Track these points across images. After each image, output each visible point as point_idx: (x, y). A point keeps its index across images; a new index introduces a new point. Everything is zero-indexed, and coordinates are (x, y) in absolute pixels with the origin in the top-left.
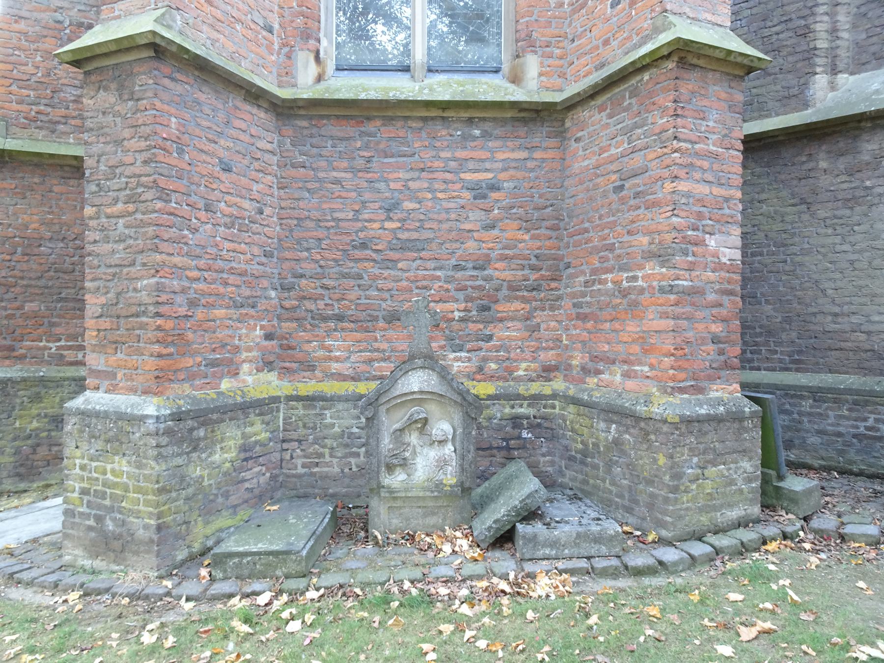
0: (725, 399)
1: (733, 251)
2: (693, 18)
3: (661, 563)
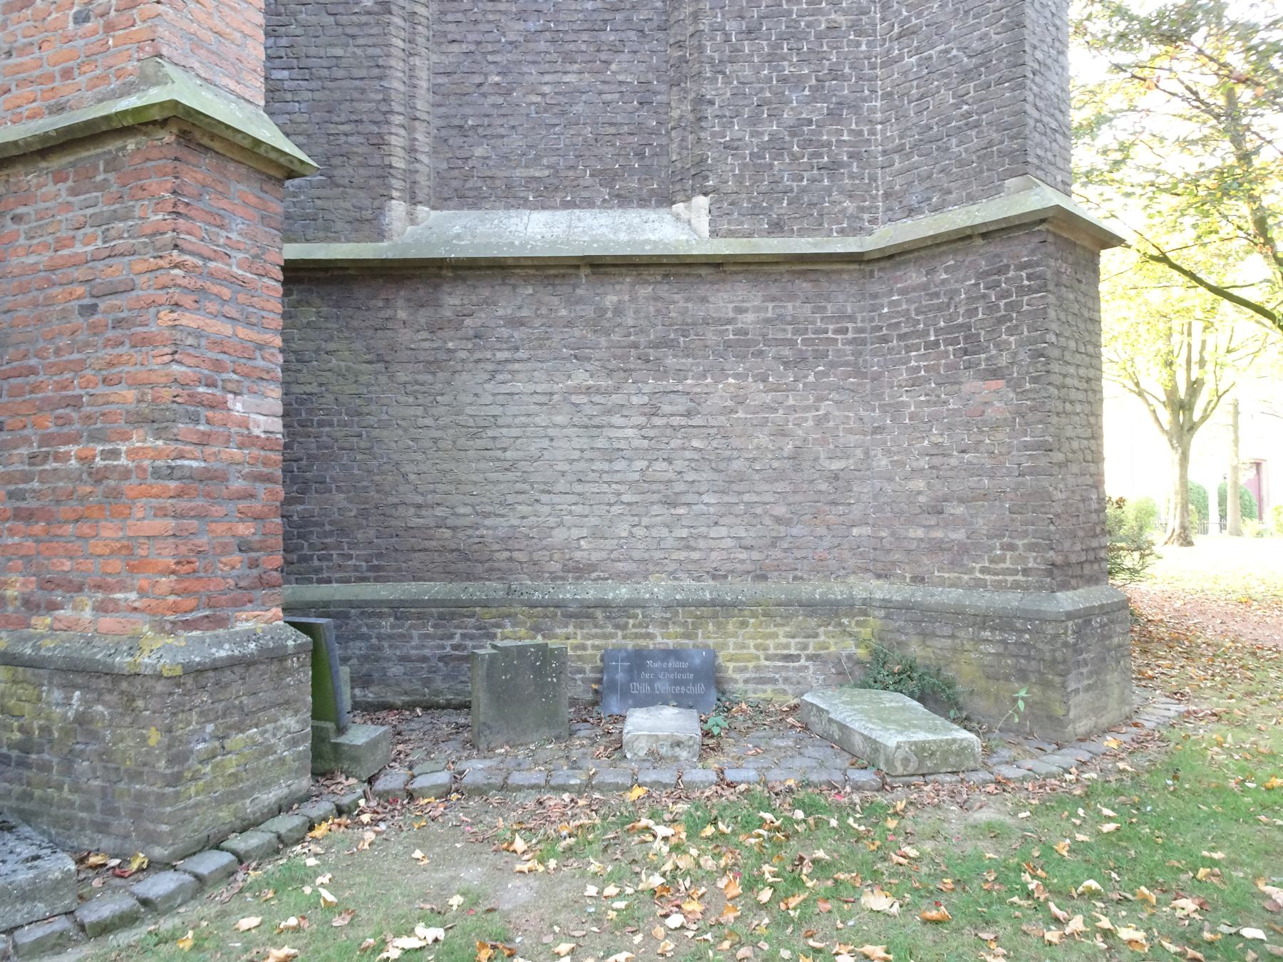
0: (259, 631)
1: (270, 419)
2: (206, 79)
3: (145, 902)
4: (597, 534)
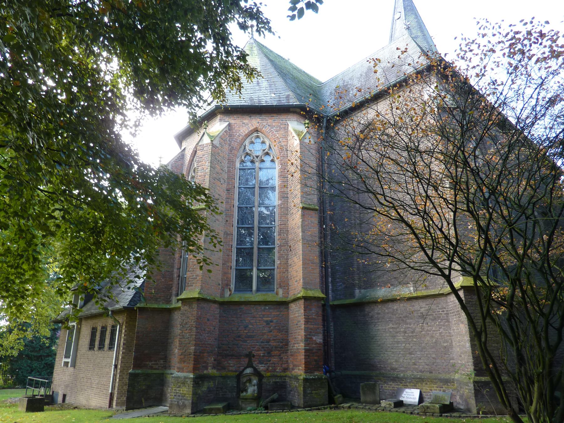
4: (396, 361)
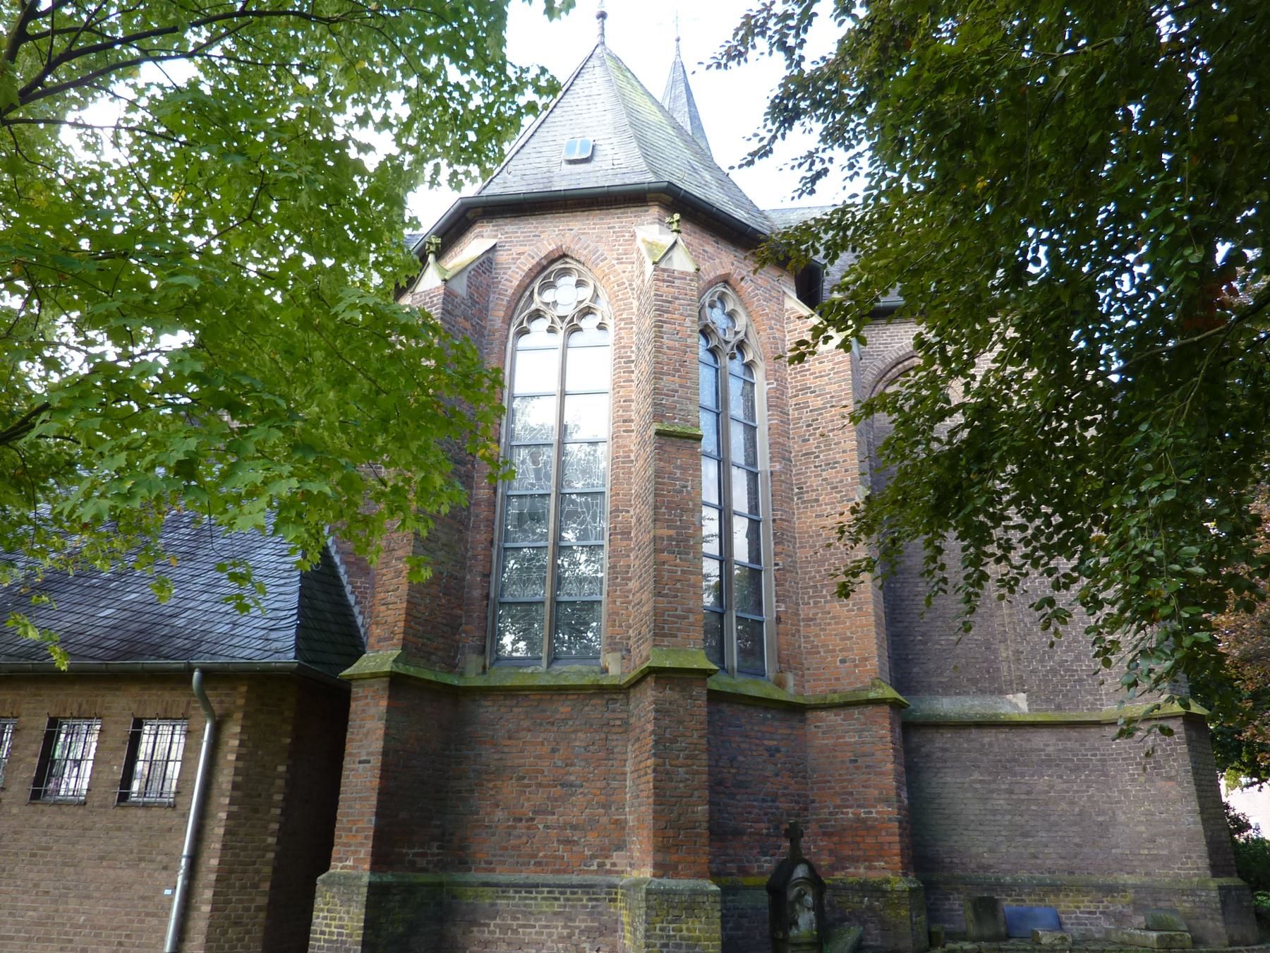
4: (991, 850)
